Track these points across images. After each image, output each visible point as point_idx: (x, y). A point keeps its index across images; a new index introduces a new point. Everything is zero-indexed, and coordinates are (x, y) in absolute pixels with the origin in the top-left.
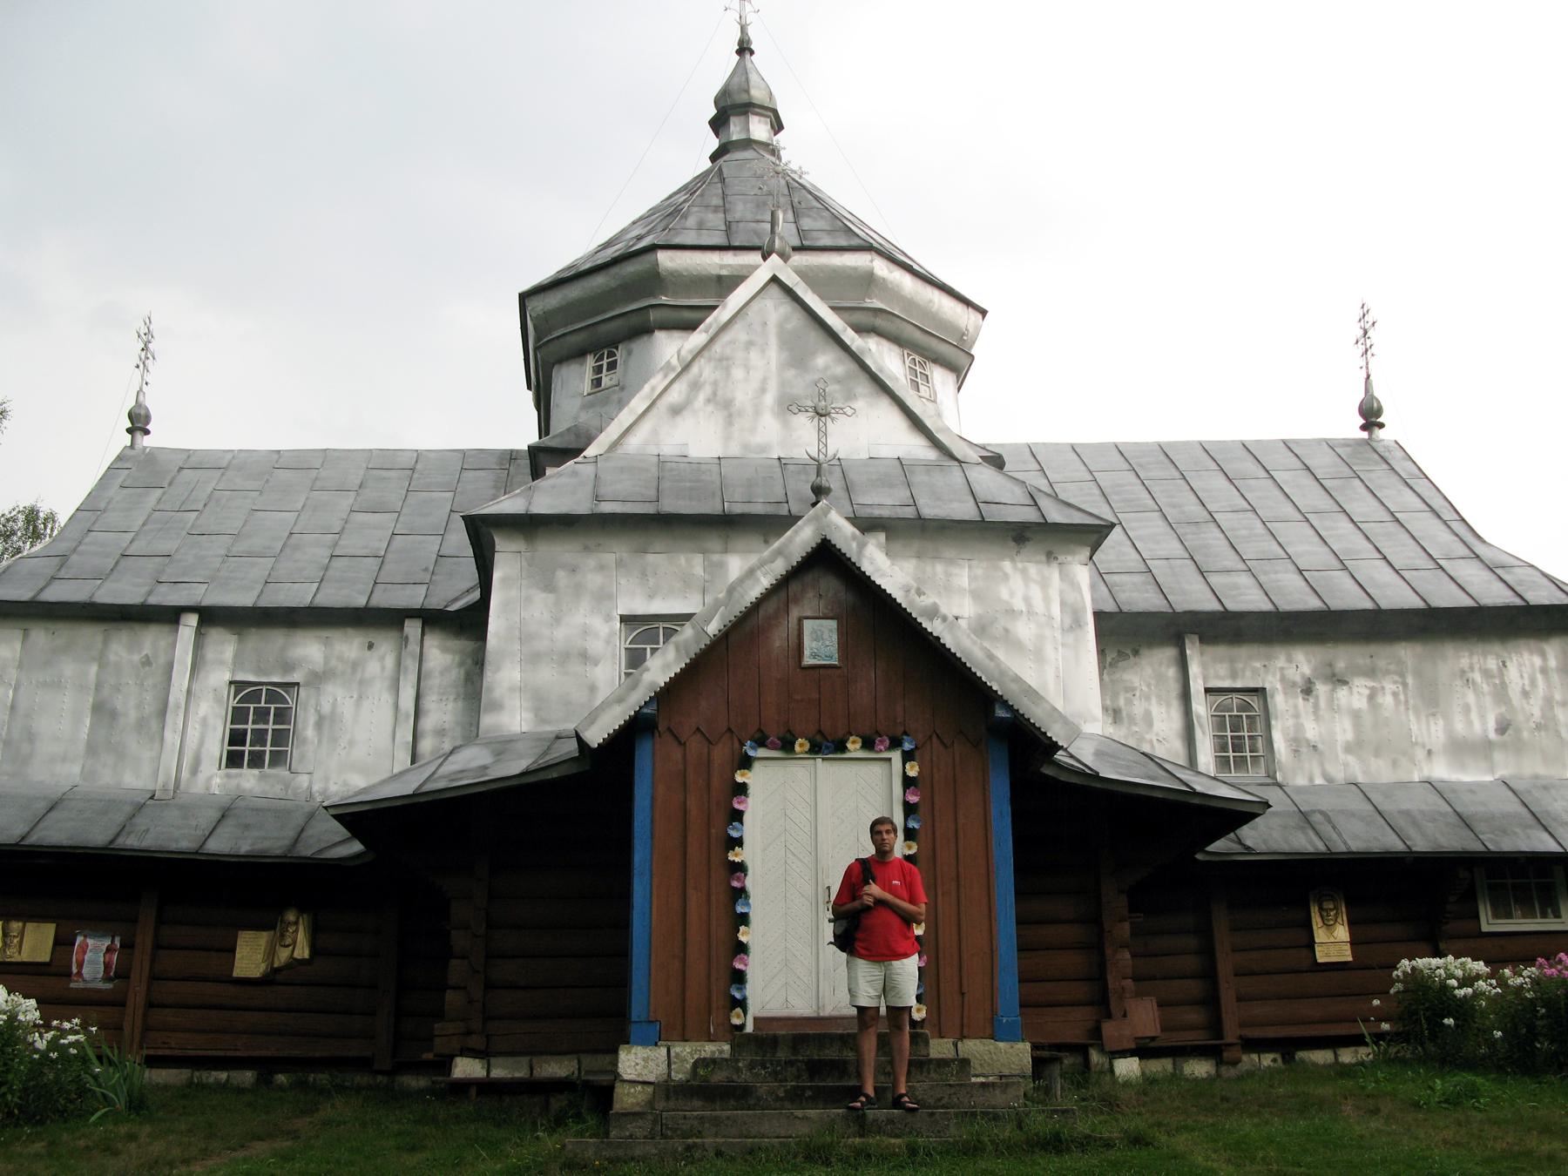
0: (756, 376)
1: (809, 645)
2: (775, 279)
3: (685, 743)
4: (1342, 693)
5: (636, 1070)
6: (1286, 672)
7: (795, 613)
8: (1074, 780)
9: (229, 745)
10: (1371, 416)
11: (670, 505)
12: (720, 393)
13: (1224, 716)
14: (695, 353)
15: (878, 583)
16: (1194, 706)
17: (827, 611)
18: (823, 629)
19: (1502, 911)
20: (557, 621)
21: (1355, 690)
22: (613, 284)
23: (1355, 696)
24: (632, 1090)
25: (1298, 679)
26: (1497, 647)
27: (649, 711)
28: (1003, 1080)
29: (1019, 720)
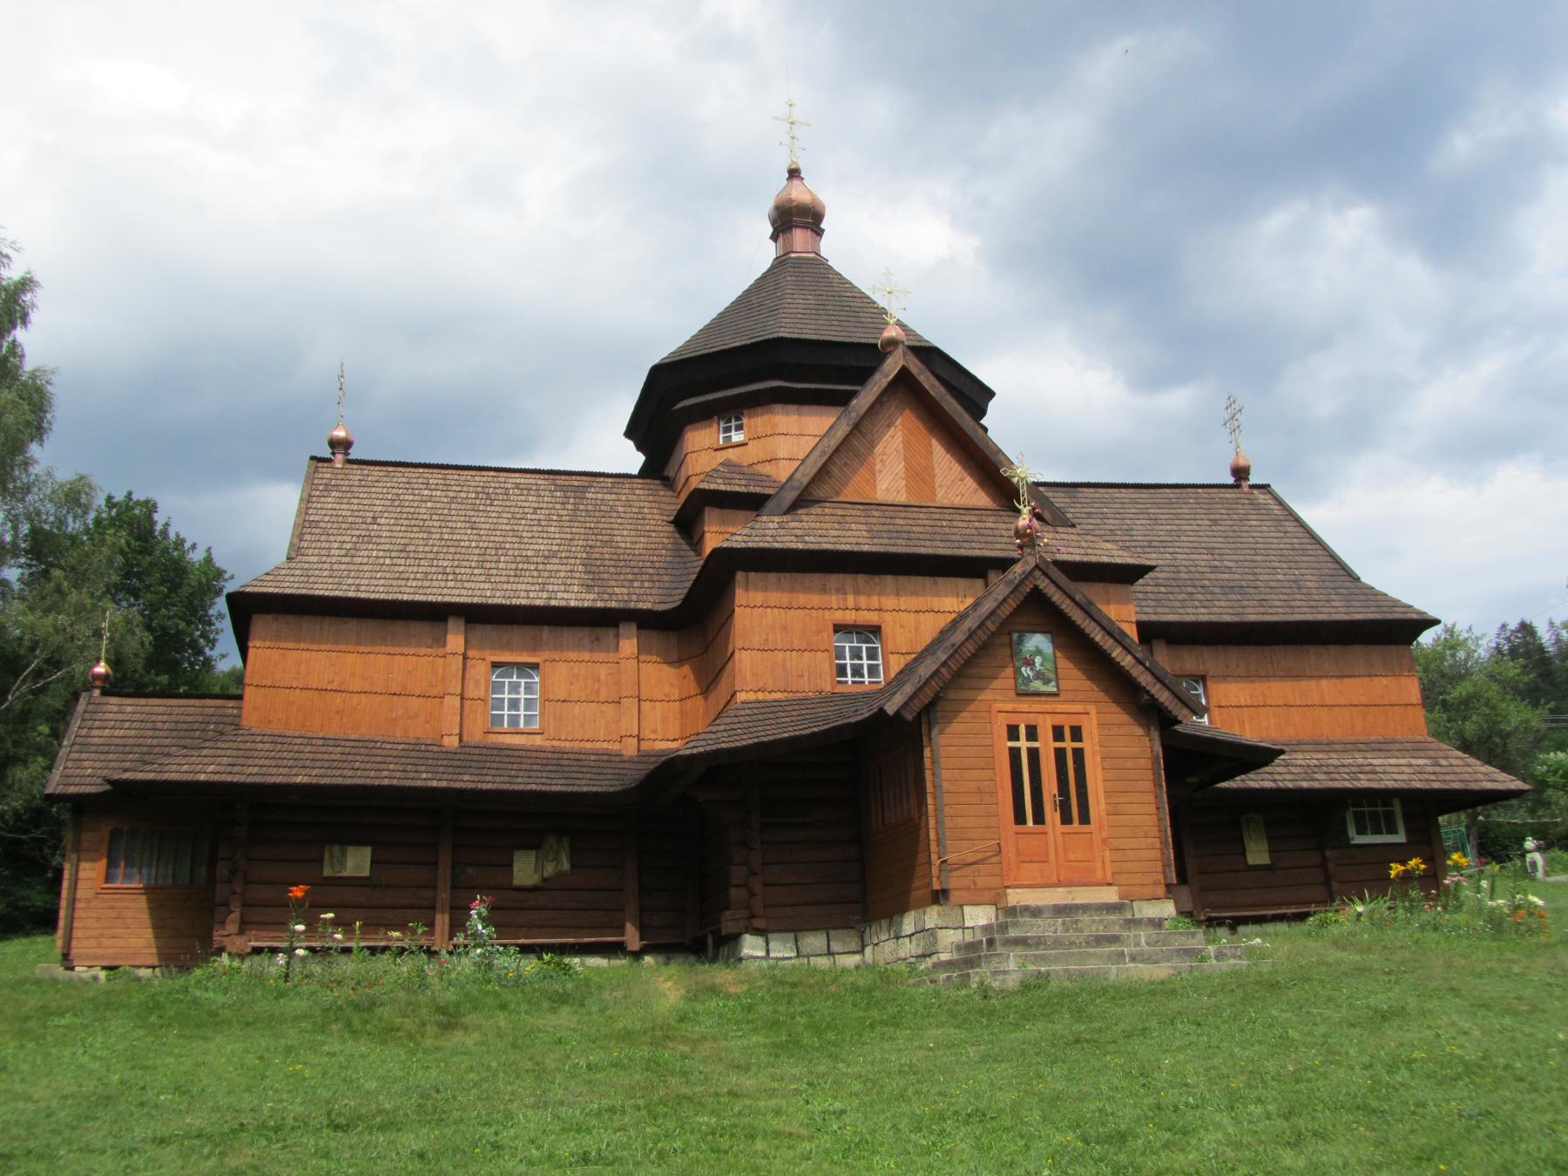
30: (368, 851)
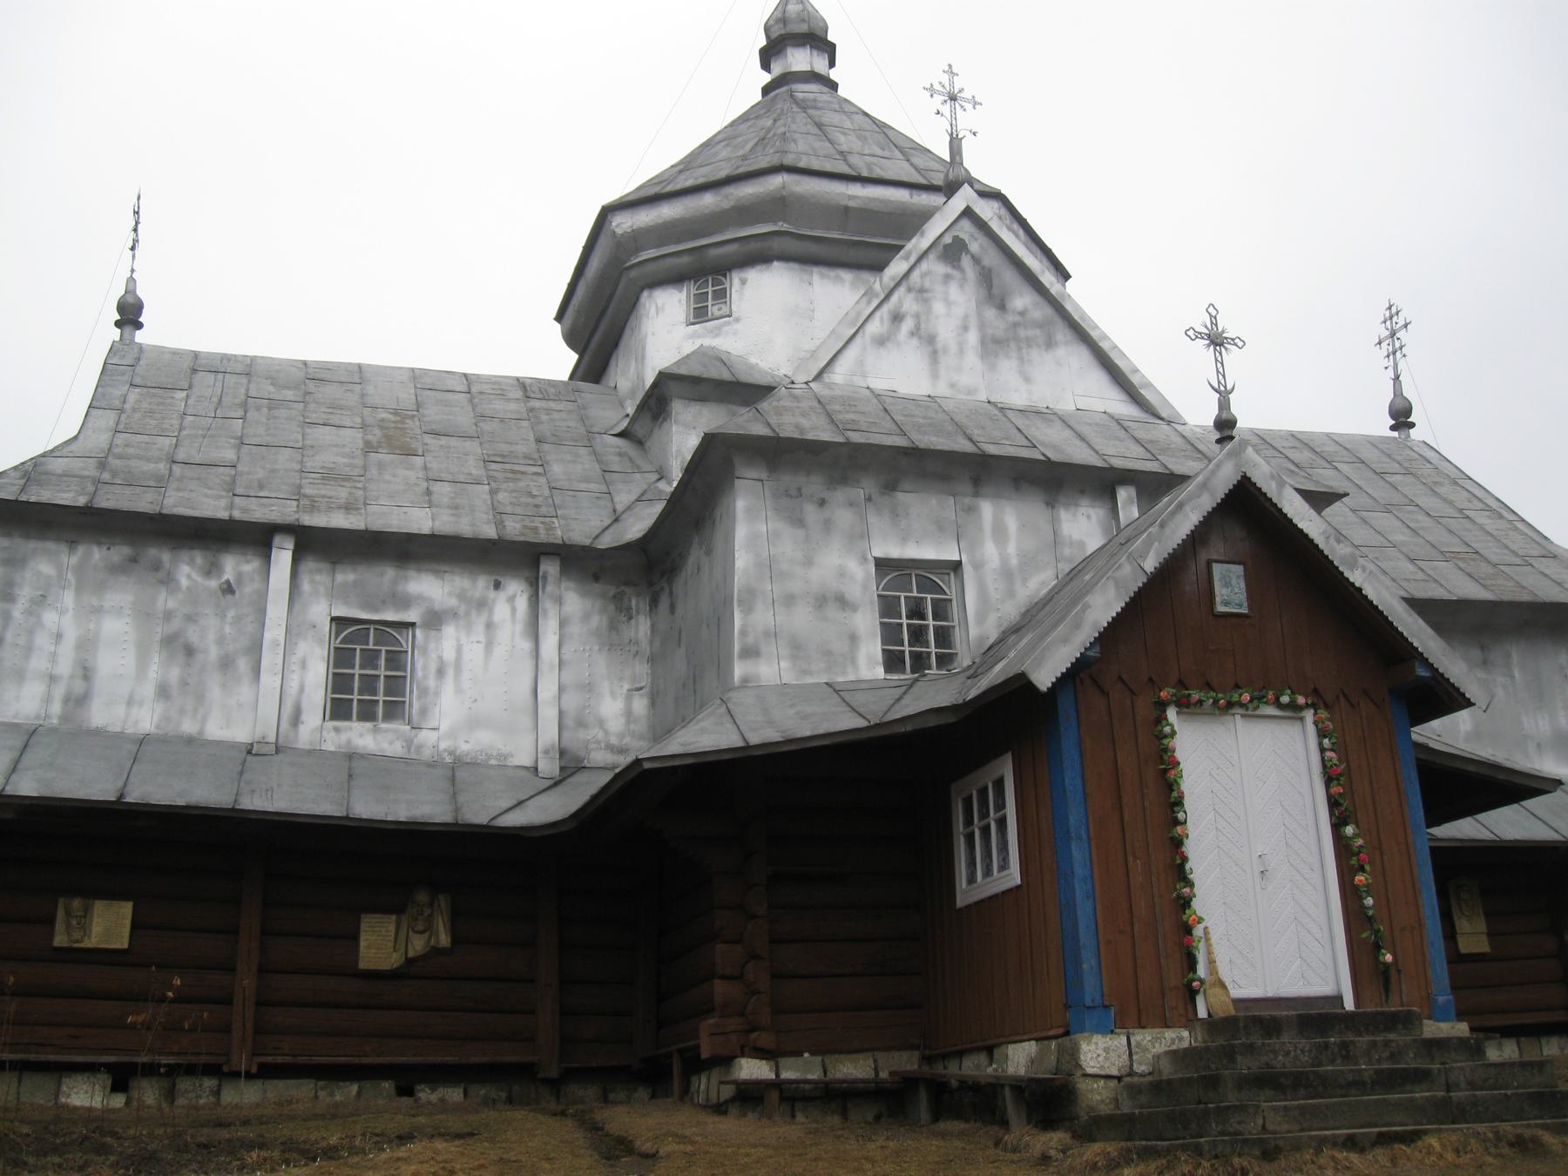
0: (959, 311)
1: (1220, 592)
2: (968, 213)
5: (1099, 1062)
9: (333, 693)
10: (1402, 417)
11: (112, 499)
12: (923, 326)
14: (897, 281)
15: (1300, 526)
18: (1231, 575)
20: (808, 562)
22: (726, 205)
27: (1092, 654)
30: (127, 908)
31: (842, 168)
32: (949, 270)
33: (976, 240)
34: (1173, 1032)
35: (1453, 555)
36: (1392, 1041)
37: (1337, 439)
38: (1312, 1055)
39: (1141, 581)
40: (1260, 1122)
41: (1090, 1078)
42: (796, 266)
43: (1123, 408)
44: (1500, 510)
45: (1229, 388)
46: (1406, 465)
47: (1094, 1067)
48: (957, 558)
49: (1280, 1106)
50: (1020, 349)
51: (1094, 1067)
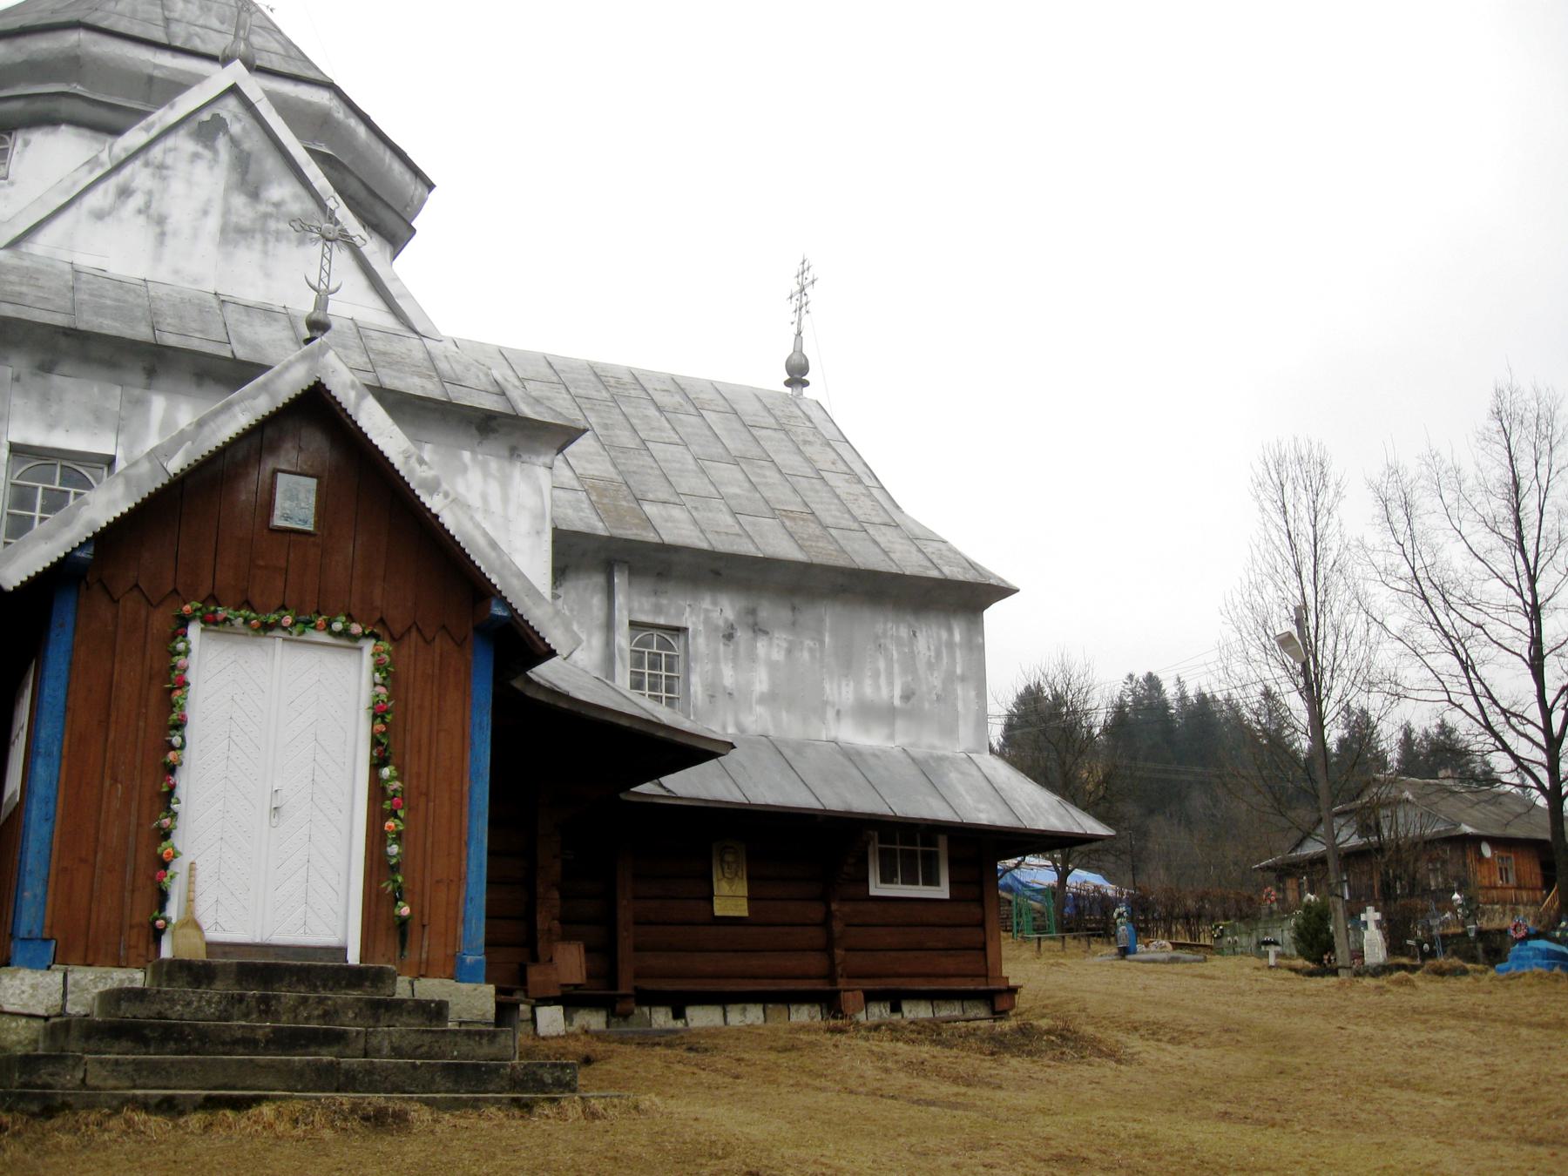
1: (282, 504)
2: (234, 90)
3: (118, 601)
4: (761, 646)
5: (22, 999)
6: (711, 614)
7: (269, 464)
8: (541, 697)
10: (797, 374)
12: (154, 205)
13: (644, 652)
14: (130, 153)
15: (375, 442)
16: (617, 638)
17: (305, 467)
19: (887, 878)
21: (776, 641)
23: (771, 649)
24: (14, 1025)
25: (721, 623)
26: (910, 618)
28: (464, 1028)
29: (516, 621)
31: (158, 35)
32: (200, 149)
33: (240, 120)
34: (124, 973)
35: (784, 513)
36: (329, 998)
37: (719, 388)
38: (221, 1007)
39: (160, 481)
40: (81, 1075)
41: (7, 1016)
42: (87, 133)
43: (389, 322)
44: (863, 478)
45: (332, 287)
46: (784, 421)
47: (14, 1004)
48: (111, 452)
49: (109, 1059)
50: (265, 242)
51: (14, 1004)
